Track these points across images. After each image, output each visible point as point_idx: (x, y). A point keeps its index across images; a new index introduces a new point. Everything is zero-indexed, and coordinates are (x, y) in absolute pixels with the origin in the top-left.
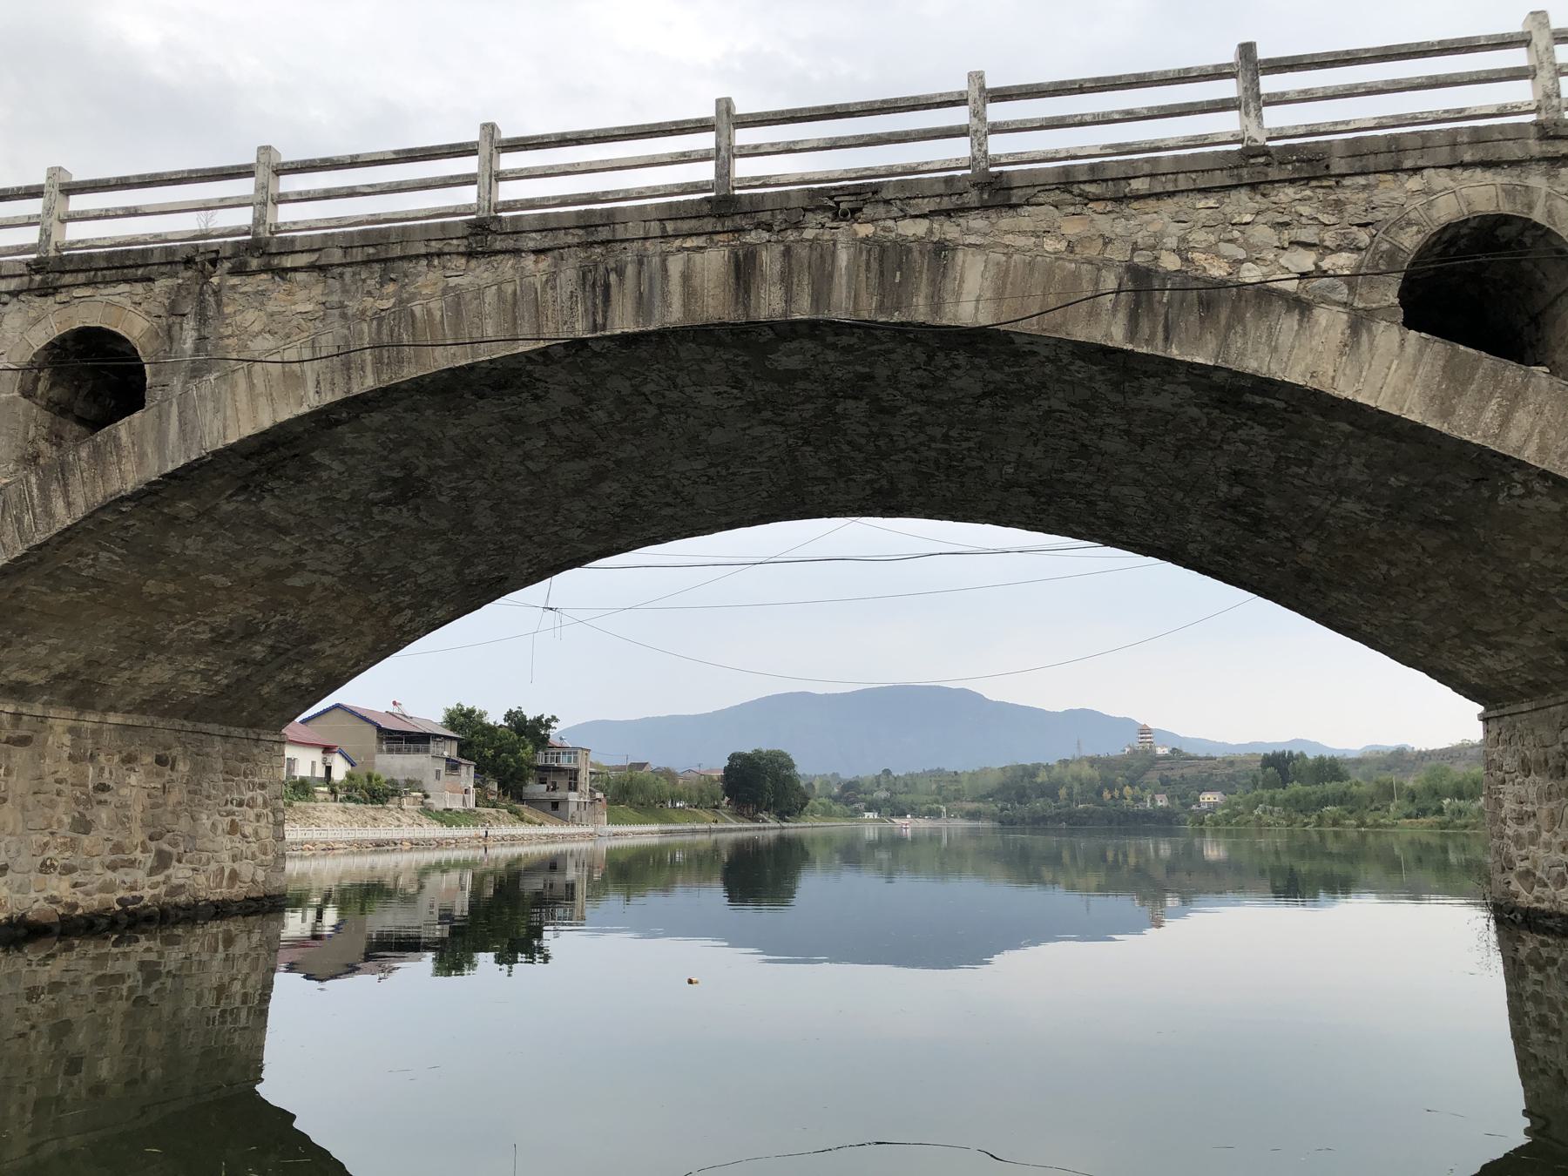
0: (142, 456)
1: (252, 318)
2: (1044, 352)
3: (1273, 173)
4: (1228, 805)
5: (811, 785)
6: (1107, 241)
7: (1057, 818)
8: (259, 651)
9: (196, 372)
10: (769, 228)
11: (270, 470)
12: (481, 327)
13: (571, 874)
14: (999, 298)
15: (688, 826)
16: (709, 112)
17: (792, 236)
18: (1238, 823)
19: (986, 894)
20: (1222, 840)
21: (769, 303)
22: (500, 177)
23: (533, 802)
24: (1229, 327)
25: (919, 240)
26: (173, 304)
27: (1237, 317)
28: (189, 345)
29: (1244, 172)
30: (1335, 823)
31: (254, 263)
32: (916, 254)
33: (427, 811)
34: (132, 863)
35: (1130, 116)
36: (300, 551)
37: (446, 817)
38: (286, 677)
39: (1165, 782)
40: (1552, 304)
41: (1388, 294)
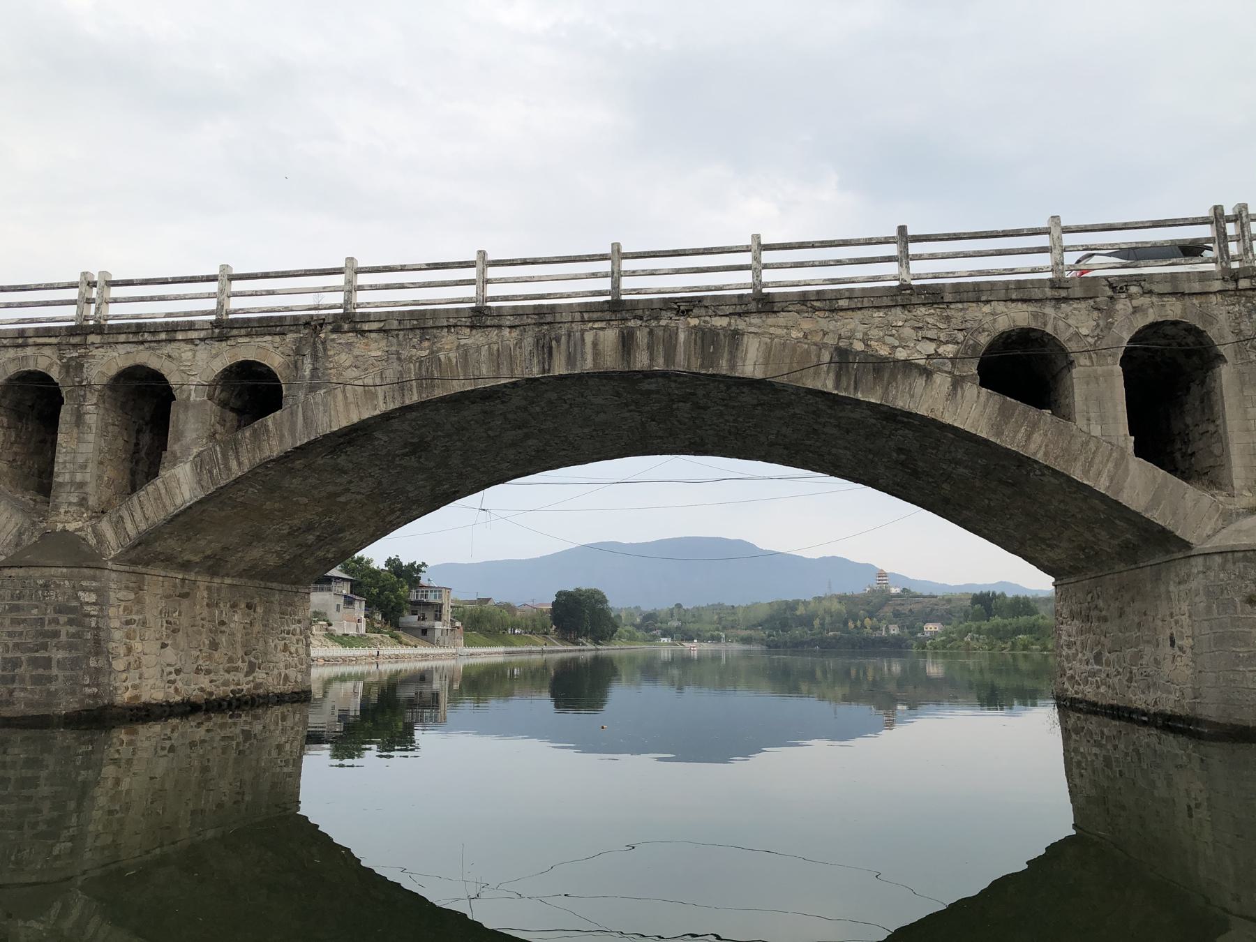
0: (282, 437)
1: (344, 358)
2: (790, 390)
3: (915, 300)
4: (946, 633)
5: (619, 616)
6: (825, 334)
7: (811, 643)
8: (311, 538)
9: (313, 389)
10: (641, 318)
11: (349, 443)
12: (479, 369)
13: (436, 685)
14: (766, 364)
15: (526, 648)
16: (607, 250)
17: (654, 323)
18: (951, 648)
19: (755, 703)
20: (940, 661)
21: (641, 361)
22: (488, 281)
23: (409, 630)
24: (889, 383)
25: (723, 328)
26: (298, 348)
27: (893, 377)
28: (307, 373)
29: (899, 298)
30: (1025, 647)
31: (346, 327)
32: (722, 337)
33: (330, 636)
34: (237, 669)
35: (839, 263)
36: (350, 482)
37: (345, 640)
38: (321, 554)
39: (897, 615)
40: (1060, 371)
41: (972, 369)
